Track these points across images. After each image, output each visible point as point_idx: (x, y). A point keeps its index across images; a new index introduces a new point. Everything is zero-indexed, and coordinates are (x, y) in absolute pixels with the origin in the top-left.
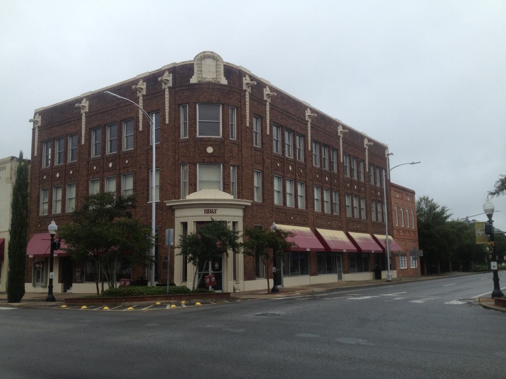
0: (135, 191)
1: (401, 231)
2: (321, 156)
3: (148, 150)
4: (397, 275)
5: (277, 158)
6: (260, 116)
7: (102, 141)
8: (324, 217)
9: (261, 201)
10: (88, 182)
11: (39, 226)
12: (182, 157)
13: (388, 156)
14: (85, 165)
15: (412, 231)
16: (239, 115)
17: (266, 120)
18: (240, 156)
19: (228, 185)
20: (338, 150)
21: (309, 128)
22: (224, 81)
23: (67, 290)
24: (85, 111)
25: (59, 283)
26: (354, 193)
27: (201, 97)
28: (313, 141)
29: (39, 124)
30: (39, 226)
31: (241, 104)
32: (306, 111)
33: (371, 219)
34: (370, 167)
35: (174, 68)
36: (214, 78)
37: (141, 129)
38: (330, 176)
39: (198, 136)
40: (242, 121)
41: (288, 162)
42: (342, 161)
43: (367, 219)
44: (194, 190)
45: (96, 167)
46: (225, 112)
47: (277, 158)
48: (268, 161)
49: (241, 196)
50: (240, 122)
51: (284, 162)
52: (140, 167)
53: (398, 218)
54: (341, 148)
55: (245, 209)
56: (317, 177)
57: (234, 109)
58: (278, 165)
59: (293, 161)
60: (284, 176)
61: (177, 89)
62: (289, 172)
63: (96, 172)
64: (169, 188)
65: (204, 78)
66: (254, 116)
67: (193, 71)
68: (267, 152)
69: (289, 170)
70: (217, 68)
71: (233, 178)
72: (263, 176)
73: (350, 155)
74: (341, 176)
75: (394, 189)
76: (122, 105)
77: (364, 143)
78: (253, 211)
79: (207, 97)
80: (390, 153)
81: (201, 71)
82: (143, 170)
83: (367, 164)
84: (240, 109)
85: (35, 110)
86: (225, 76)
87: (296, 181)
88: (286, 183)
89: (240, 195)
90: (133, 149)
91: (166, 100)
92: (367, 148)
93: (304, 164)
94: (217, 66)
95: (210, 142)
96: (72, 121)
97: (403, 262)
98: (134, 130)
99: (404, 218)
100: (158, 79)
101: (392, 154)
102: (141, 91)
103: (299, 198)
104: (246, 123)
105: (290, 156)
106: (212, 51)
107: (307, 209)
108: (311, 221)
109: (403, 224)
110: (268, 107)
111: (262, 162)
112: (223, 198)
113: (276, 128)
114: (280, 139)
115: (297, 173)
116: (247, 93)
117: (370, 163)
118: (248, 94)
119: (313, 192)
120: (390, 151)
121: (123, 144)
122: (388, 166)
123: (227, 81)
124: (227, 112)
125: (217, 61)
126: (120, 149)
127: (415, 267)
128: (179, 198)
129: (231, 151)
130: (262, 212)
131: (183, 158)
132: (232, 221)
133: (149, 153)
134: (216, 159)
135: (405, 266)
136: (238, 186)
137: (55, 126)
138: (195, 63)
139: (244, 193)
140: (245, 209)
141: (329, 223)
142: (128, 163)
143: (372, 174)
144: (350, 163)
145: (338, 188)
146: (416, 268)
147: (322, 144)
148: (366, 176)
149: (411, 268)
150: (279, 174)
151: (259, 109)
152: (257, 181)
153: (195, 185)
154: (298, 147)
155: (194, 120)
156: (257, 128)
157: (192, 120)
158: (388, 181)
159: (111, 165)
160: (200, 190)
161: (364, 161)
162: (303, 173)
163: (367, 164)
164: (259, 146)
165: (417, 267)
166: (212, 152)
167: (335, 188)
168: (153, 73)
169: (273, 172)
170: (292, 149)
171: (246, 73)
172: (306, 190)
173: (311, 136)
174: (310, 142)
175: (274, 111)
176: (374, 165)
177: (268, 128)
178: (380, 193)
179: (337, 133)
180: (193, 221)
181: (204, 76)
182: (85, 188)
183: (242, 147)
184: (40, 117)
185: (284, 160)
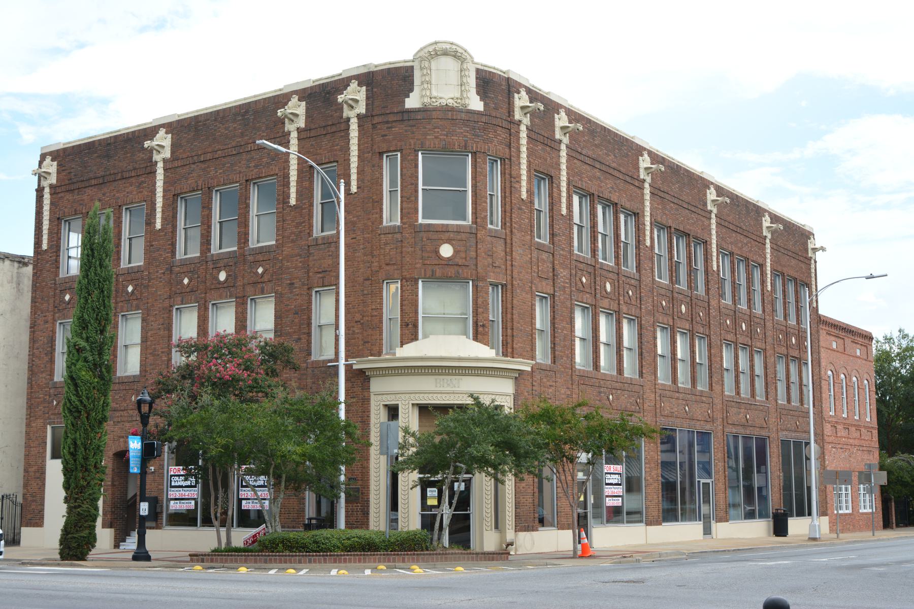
0: (280, 336)
1: (839, 427)
2: (671, 258)
3: (309, 246)
4: (830, 527)
5: (582, 266)
6: (547, 175)
7: (203, 223)
8: (677, 395)
9: (549, 362)
10: (170, 311)
11: (55, 403)
12: (387, 264)
13: (814, 253)
14: (164, 273)
15: (865, 427)
16: (507, 176)
17: (560, 183)
18: (509, 263)
19: (483, 326)
20: (706, 243)
21: (647, 197)
22: (476, 104)
23: (121, 543)
24: (162, 156)
25: (103, 527)
26: (741, 339)
27: (428, 137)
28: (655, 223)
29: (53, 180)
30: (55, 403)
31: (510, 153)
32: (641, 158)
33: (776, 400)
34: (775, 280)
35: (371, 75)
36: (457, 98)
37: (293, 201)
38: (690, 303)
39: (421, 220)
40: (513, 188)
41: (604, 273)
42: (715, 268)
43: (767, 399)
44: (413, 337)
45: (188, 278)
46: (478, 169)
47: (582, 266)
48: (563, 273)
49: (510, 350)
50: (508, 190)
51: (595, 274)
52: (290, 284)
53: (834, 396)
54: (714, 237)
55: (519, 377)
56: (662, 304)
57: (496, 161)
58: (584, 280)
59: (614, 271)
60: (595, 306)
61: (376, 120)
62: (606, 295)
63: (188, 290)
64: (357, 331)
65: (435, 98)
66: (574, 191)
67: (412, 83)
68: (561, 252)
69: (606, 291)
70: (461, 76)
71: (495, 313)
72: (553, 307)
73: (732, 254)
74: (713, 303)
75: (825, 330)
76: (251, 147)
77: (761, 224)
78: (534, 383)
79: (442, 137)
80: (818, 246)
81: (429, 83)
82: (296, 291)
83: (769, 272)
84: (509, 163)
85: (42, 148)
86: (478, 93)
87: (619, 314)
88: (599, 320)
89: (508, 350)
90: (274, 243)
91: (351, 143)
92: (769, 236)
93: (637, 277)
94: (463, 74)
95: (447, 235)
96: (131, 177)
97: (844, 498)
98: (279, 204)
99: (847, 396)
100: (337, 99)
101: (823, 249)
102: (295, 120)
103: (602, 348)
104: (520, 191)
105: (606, 260)
106: (451, 40)
107: (642, 378)
108: (649, 404)
109: (845, 411)
110: (563, 153)
111: (551, 274)
112: (473, 355)
113: (577, 197)
114: (587, 223)
115: (621, 298)
116: (523, 128)
117: (774, 270)
118: (525, 129)
119: (655, 338)
120: (818, 241)
121: (250, 232)
122: (813, 275)
123: (482, 103)
124: (482, 169)
125: (462, 62)
126: (244, 243)
127: (871, 511)
128: (380, 353)
129: (490, 253)
130: (551, 384)
131: (388, 268)
132: (398, 404)
133: (312, 253)
134: (460, 271)
135: (847, 508)
136: (505, 328)
137: (92, 186)
138: (416, 65)
139: (516, 344)
140: (519, 377)
141: (687, 408)
142: (263, 273)
143: (779, 294)
144: (733, 271)
145: (707, 330)
146: (872, 513)
147: (673, 229)
148: (766, 301)
149: (861, 511)
150: (585, 301)
151: (546, 160)
152: (541, 318)
153: (416, 326)
154: (623, 238)
155: (413, 186)
156: (542, 203)
157: (410, 186)
158: (815, 310)
159: (222, 276)
160: (425, 336)
161: (762, 266)
162: (634, 297)
163: (769, 272)
164: (545, 240)
165: (874, 510)
166: (452, 256)
167: (701, 330)
168: (321, 82)
169: (573, 298)
170: (611, 244)
171: (521, 85)
172: (640, 336)
173: (651, 213)
174: (648, 228)
175: (575, 161)
176: (783, 275)
177: (564, 200)
178: (796, 339)
179: (705, 204)
180: (411, 402)
181: (434, 94)
182: (163, 324)
183: (512, 244)
184: (55, 163)
185: (595, 270)
